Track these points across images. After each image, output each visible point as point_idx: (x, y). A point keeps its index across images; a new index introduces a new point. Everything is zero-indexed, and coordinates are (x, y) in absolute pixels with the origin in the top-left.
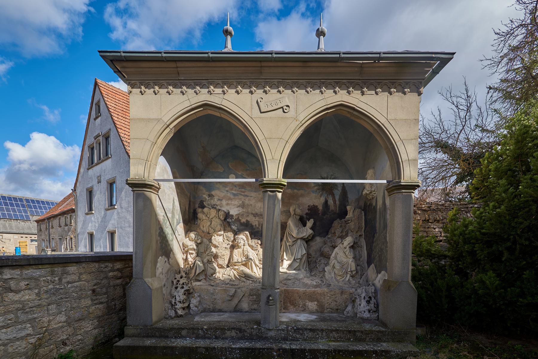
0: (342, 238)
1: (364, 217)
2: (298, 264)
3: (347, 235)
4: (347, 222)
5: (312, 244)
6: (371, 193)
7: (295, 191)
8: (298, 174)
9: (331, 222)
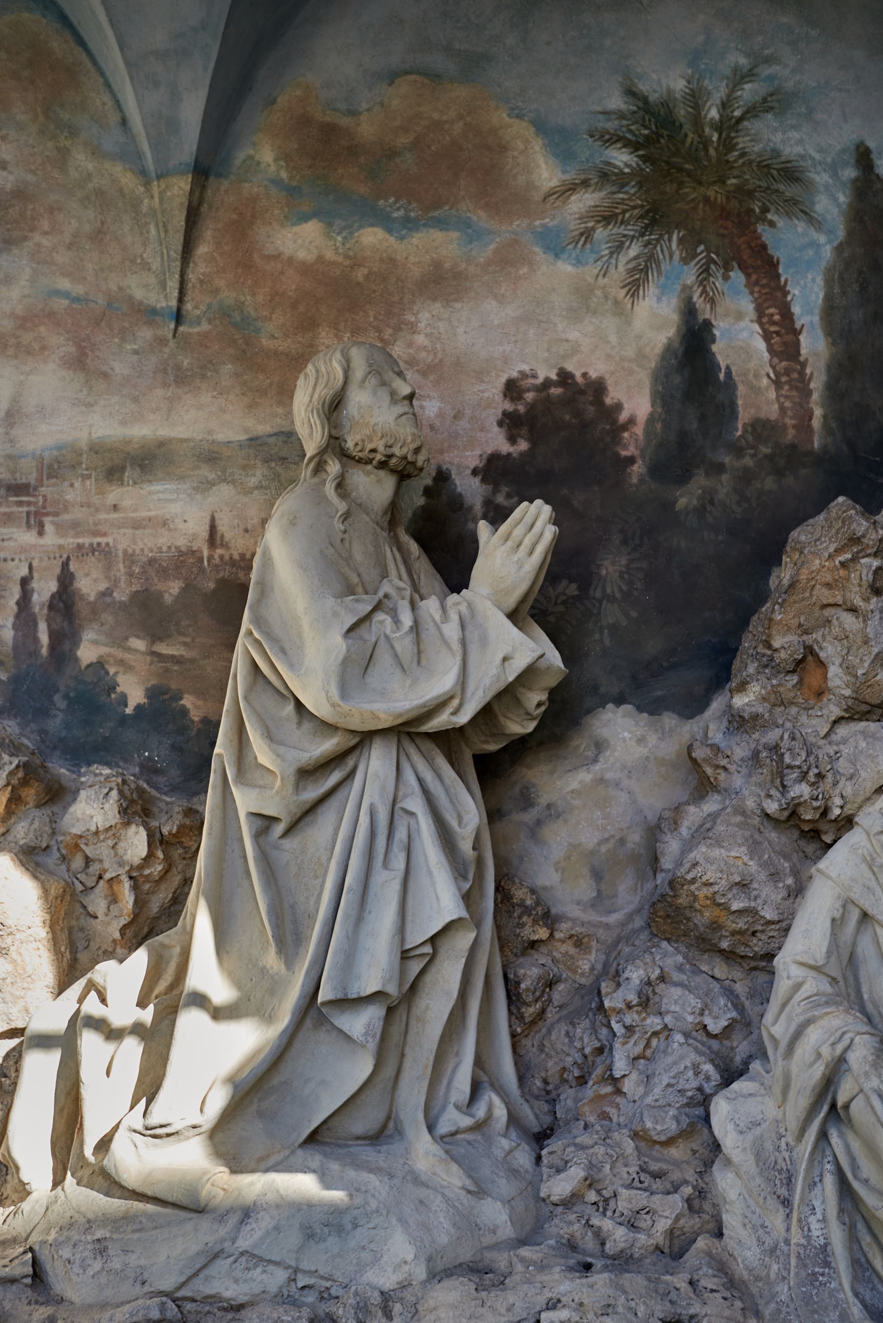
2: (364, 1068)
5: (561, 783)
7: (372, 237)
8: (392, 77)
9: (765, 546)
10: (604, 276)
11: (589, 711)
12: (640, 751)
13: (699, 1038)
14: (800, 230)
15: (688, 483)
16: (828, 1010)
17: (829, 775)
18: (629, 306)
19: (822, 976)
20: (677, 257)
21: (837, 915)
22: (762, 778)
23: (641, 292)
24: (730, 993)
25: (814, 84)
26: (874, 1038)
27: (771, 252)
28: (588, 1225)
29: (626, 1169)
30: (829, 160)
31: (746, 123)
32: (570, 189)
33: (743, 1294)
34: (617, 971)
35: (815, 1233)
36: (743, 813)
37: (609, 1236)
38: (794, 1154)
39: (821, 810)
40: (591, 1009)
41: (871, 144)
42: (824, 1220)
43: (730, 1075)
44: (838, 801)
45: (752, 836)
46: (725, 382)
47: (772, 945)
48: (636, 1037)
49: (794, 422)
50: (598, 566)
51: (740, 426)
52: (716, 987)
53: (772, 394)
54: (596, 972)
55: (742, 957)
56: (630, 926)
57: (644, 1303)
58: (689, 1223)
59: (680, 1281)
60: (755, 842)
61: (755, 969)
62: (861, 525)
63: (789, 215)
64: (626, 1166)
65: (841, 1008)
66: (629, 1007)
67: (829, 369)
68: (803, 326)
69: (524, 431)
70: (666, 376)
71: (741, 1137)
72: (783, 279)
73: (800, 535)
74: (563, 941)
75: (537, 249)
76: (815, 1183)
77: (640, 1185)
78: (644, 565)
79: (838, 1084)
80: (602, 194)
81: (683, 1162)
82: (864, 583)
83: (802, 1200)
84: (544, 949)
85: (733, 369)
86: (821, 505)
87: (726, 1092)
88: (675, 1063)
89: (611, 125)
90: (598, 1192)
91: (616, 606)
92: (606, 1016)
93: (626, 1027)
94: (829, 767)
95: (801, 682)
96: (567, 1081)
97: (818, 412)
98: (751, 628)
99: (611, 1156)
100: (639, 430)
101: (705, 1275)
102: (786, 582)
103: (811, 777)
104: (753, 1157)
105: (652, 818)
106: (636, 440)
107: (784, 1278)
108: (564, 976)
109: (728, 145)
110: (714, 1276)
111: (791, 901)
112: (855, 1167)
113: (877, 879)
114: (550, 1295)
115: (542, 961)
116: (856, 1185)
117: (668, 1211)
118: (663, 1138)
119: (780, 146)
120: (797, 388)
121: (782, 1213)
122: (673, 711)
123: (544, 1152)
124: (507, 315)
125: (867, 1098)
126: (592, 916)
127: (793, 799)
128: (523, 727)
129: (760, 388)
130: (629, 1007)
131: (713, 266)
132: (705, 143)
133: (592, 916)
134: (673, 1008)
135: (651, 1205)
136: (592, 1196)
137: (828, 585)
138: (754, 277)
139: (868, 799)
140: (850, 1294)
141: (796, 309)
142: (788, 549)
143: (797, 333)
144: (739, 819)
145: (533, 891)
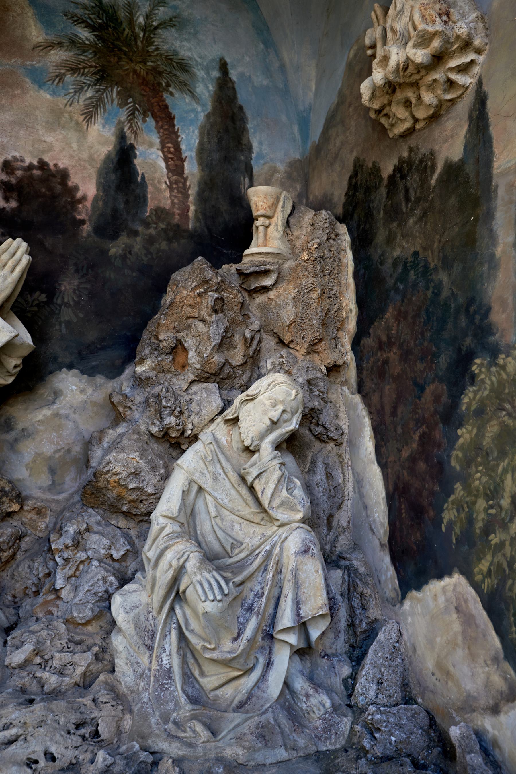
0: (230, 378)
3: (253, 366)
4: (252, 283)
6: (438, 59)
9: (156, 284)
10: (70, 105)
11: (51, 372)
12: (82, 397)
13: (108, 562)
14: (187, 101)
15: (117, 240)
16: (177, 541)
17: (186, 412)
18: (85, 127)
20: (116, 102)
22: (150, 413)
23: (93, 120)
24: (127, 536)
25: (199, 17)
26: (200, 554)
27: (170, 110)
28: (34, 677)
29: (60, 642)
30: (205, 64)
31: (159, 31)
32: (50, 46)
33: (124, 702)
34: (61, 527)
36: (139, 433)
37: (46, 682)
38: (156, 621)
39: (181, 431)
40: (44, 551)
41: (228, 60)
42: (170, 655)
43: (124, 581)
44: (190, 426)
45: (142, 446)
46: (141, 183)
47: (151, 507)
48: (70, 565)
49: (179, 212)
50: (60, 285)
51: (149, 210)
52: (119, 533)
53: (168, 194)
54: (49, 529)
55: (135, 515)
56: (71, 501)
57: (64, 716)
58: (95, 667)
59: (87, 701)
60: (144, 450)
61: (142, 521)
62: (209, 274)
63: (181, 91)
64: (60, 640)
65: (184, 539)
66: (67, 547)
67: (199, 184)
68: (186, 157)
69: (15, 195)
70: (106, 174)
71: (127, 616)
72: (176, 128)
73: (177, 276)
74: (29, 512)
75: (27, 80)
76: (166, 635)
77: (67, 650)
78: (88, 286)
80: (71, 54)
82: (209, 306)
83: (159, 645)
84: (16, 517)
85: (146, 175)
86: (190, 261)
87: (121, 591)
88: (92, 578)
89: (79, 12)
90: (42, 657)
91: (70, 309)
92: (53, 554)
93: (64, 559)
94: (186, 407)
95: (174, 360)
96: (28, 595)
97: (192, 208)
98: (148, 328)
99: (51, 635)
100: (88, 204)
101: (102, 695)
102: (168, 302)
103: (176, 413)
104: (133, 625)
105: (87, 436)
106: (87, 210)
107: (146, 689)
108: (29, 532)
109: (149, 41)
110: (108, 694)
111: (163, 482)
113: (207, 468)
114: (5, 721)
115: (15, 524)
116: (187, 633)
117: (83, 661)
118: (83, 621)
119: (178, 49)
120: (181, 192)
122: (103, 374)
123: (9, 638)
124: (5, 118)
125: (194, 586)
126: (49, 496)
128: (5, 380)
129: (161, 189)
130: (67, 547)
131: (137, 112)
132: (136, 37)
133: (49, 496)
135: (74, 660)
136: (38, 660)
137: (191, 306)
138: (160, 123)
139: (206, 425)
140: (180, 692)
141: (183, 147)
142: (170, 283)
143: (183, 160)
144: (136, 436)
145: (10, 482)
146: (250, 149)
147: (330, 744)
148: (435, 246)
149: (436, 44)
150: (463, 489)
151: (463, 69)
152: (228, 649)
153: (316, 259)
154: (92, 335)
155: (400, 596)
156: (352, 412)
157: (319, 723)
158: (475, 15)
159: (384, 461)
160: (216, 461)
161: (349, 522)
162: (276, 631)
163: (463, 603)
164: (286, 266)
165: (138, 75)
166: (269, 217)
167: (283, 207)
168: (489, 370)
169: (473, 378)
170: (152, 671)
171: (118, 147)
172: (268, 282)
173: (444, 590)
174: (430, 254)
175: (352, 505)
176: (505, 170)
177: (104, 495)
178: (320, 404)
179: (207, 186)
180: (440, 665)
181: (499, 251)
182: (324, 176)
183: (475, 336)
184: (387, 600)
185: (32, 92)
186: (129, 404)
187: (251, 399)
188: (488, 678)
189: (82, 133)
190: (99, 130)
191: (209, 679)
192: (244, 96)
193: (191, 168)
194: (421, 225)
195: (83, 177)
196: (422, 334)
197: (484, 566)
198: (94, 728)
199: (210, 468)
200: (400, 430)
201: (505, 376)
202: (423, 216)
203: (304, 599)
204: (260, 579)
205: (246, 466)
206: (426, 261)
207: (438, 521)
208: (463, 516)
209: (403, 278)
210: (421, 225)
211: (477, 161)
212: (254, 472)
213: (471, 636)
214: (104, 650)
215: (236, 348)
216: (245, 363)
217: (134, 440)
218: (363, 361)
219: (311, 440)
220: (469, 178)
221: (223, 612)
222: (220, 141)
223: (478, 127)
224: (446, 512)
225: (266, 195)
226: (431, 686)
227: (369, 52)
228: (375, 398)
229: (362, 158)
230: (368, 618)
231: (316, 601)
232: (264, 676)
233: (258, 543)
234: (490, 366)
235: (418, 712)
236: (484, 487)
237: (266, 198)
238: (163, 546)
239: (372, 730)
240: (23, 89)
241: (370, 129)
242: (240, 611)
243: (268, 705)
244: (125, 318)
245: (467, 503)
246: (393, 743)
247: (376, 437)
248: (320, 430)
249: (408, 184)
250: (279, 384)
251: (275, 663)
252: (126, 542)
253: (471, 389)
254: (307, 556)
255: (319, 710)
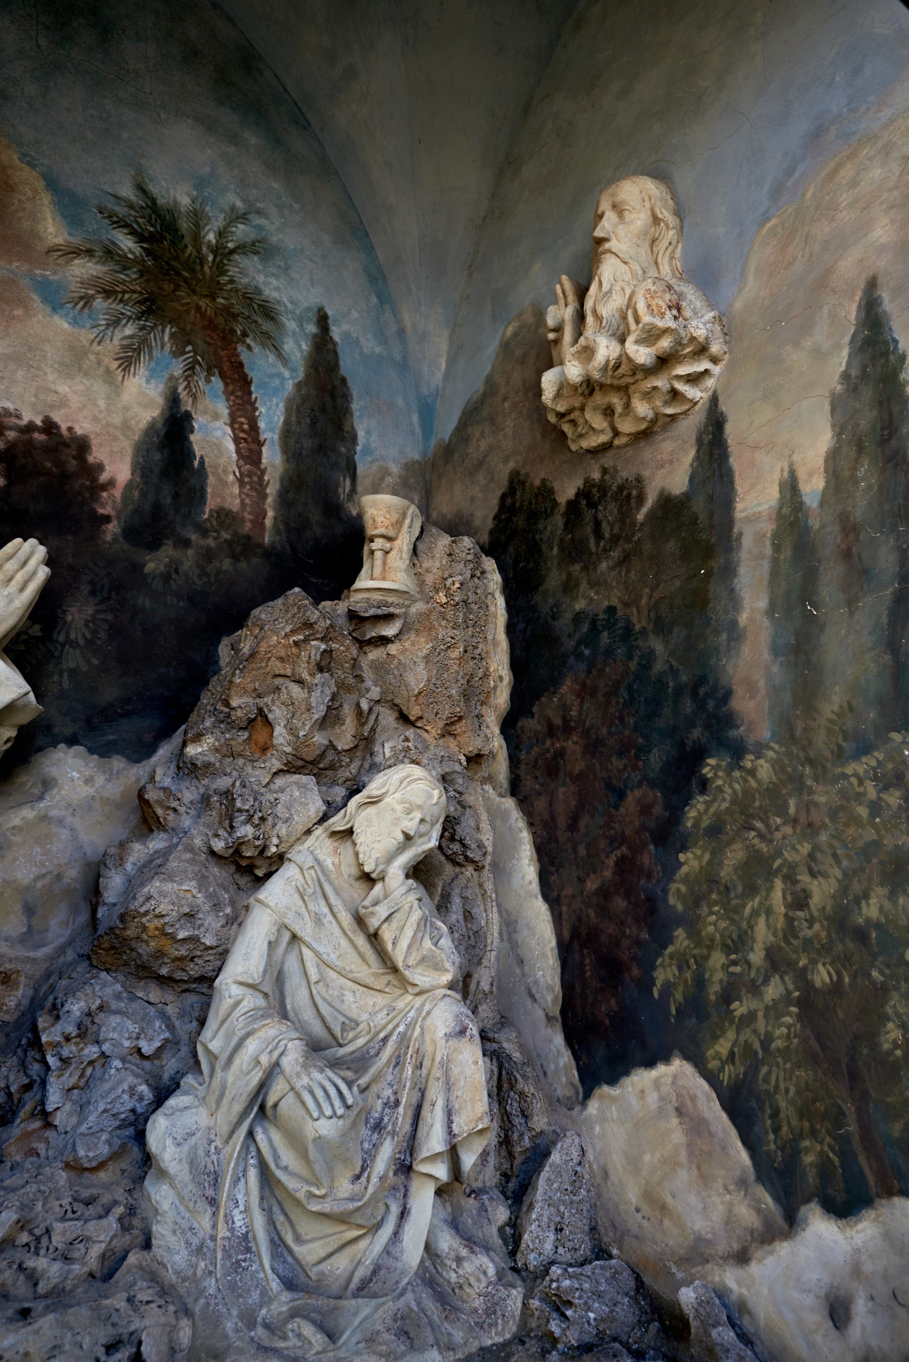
0: (339, 772)
1: (499, 605)
6: (663, 362)
10: (99, 343)
11: (40, 749)
12: (88, 791)
13: (134, 1061)
14: (270, 360)
17: (270, 818)
18: (120, 378)
19: (257, 993)
20: (168, 347)
21: (273, 939)
22: (211, 819)
24: (164, 1016)
27: (246, 370)
29: (59, 1202)
30: (298, 312)
32: (75, 252)
35: (238, 1224)
36: (192, 851)
38: (221, 1156)
41: (330, 312)
42: (247, 1210)
44: (275, 841)
48: (72, 1068)
50: (65, 612)
51: (207, 510)
52: (151, 1010)
53: (236, 491)
56: (62, 959)
57: (90, 1333)
58: (120, 1243)
59: (118, 1301)
60: (204, 877)
63: (263, 345)
64: (58, 1199)
66: (68, 1039)
67: (282, 481)
70: (148, 450)
72: (254, 396)
73: (260, 613)
75: (35, 296)
76: (239, 1179)
77: (72, 1216)
78: (110, 617)
79: (270, 1086)
80: (106, 269)
81: (112, 1184)
83: (228, 1196)
85: (206, 460)
88: (113, 1089)
89: (121, 211)
90: (31, 1232)
91: (78, 651)
93: (61, 1060)
95: (249, 738)
97: (270, 514)
99: (44, 1192)
100: (117, 493)
106: (114, 502)
107: (210, 1273)
110: (149, 1287)
112: (276, 1157)
113: (306, 906)
116: (279, 1173)
117: (103, 1233)
118: (94, 1164)
119: (262, 287)
121: (209, 1211)
122: (123, 755)
125: (298, 1096)
126: (21, 952)
127: (238, 838)
130: (68, 1039)
131: (198, 367)
132: (202, 260)
133: (21, 952)
134: (111, 1035)
135: (85, 1233)
136: (24, 1238)
137: (281, 659)
138: (231, 387)
139: (299, 839)
140: (269, 1272)
141: (262, 425)
143: (261, 444)
144: (188, 856)
146: (354, 439)
147: (496, 1334)
148: (643, 602)
149: (665, 343)
150: (687, 938)
151: (693, 379)
152: (346, 1195)
153: (458, 604)
154: (109, 693)
155: (581, 1095)
156: (499, 823)
157: (478, 1303)
158: (712, 314)
159: (555, 894)
160: (319, 894)
161: (492, 985)
162: (419, 1159)
163: (689, 1103)
164: (413, 610)
165: (203, 315)
166: (390, 539)
167: (410, 527)
168: (729, 775)
169: (704, 785)
170: (219, 1241)
171: (167, 414)
172: (390, 631)
173: (657, 1084)
174: (635, 613)
175: (497, 958)
176: (754, 514)
177: (132, 950)
178: (456, 809)
179: (293, 485)
180: (649, 1196)
181: (743, 618)
182: (458, 488)
183: (708, 726)
184: (558, 1100)
185: (40, 316)
186: (174, 804)
187: (374, 802)
188: (730, 1211)
189: (116, 388)
190: (140, 386)
191: (310, 1246)
192: (348, 365)
193: (272, 457)
194: (620, 574)
195: (112, 451)
196: (621, 719)
197: (723, 1047)
198: (134, 1350)
199: (311, 907)
200: (582, 851)
201: (754, 784)
202: (624, 561)
203: (457, 1107)
204: (390, 1078)
205: (366, 903)
206: (628, 621)
207: (646, 983)
208: (688, 975)
209: (591, 638)
210: (620, 574)
211: (710, 498)
212: (382, 911)
213: (701, 1150)
214: (132, 1211)
215: (343, 724)
216: (356, 746)
217: (188, 861)
218: (521, 751)
219: (441, 862)
220: (697, 519)
221: (344, 1135)
222: (314, 423)
223: (711, 455)
224: (660, 970)
225: (389, 508)
226: (635, 1229)
227: (551, 336)
228: (540, 804)
229: (523, 472)
230: (531, 1129)
231: (473, 1109)
232: (396, 1234)
233: (384, 1021)
234: (730, 769)
235: (619, 1269)
236: (722, 935)
237: (388, 512)
238: (243, 1032)
239: (559, 1305)
240: (27, 308)
241: (539, 436)
242: (364, 1132)
243: (406, 1281)
244: (163, 670)
245: (695, 957)
246: (592, 1321)
247: (540, 860)
248: (456, 847)
249: (600, 516)
250: (416, 780)
251: (413, 1211)
252: (163, 1027)
253: (701, 799)
254: (463, 1040)
255: (479, 1281)
